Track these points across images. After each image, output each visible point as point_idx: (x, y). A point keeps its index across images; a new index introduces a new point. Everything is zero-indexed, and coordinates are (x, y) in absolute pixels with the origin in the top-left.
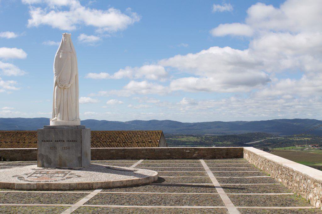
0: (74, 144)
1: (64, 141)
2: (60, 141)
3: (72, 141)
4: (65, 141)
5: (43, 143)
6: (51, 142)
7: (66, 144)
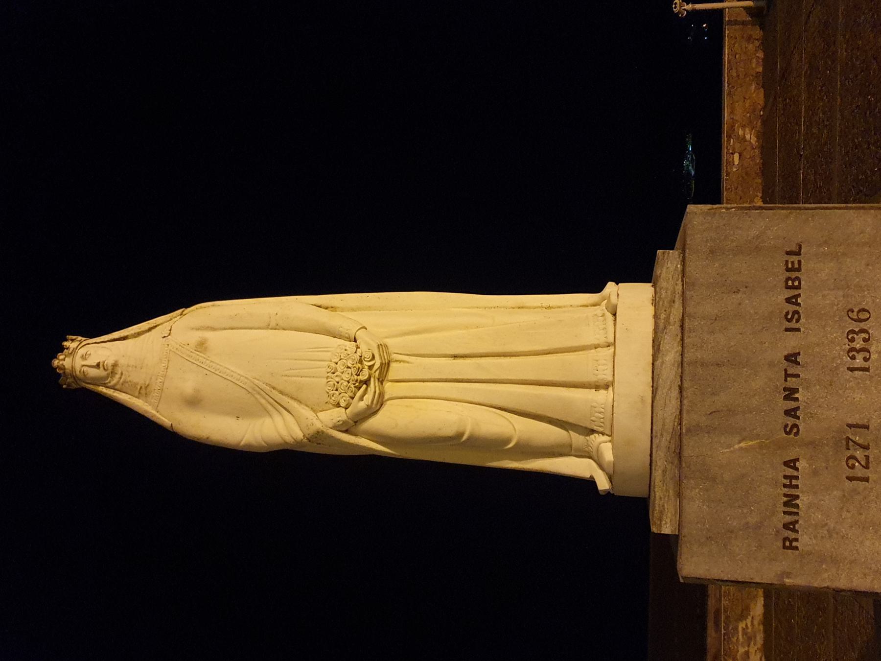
0: (816, 271)
1: (792, 358)
2: (790, 394)
3: (793, 284)
4: (791, 342)
5: (805, 540)
6: (801, 465)
7: (822, 339)
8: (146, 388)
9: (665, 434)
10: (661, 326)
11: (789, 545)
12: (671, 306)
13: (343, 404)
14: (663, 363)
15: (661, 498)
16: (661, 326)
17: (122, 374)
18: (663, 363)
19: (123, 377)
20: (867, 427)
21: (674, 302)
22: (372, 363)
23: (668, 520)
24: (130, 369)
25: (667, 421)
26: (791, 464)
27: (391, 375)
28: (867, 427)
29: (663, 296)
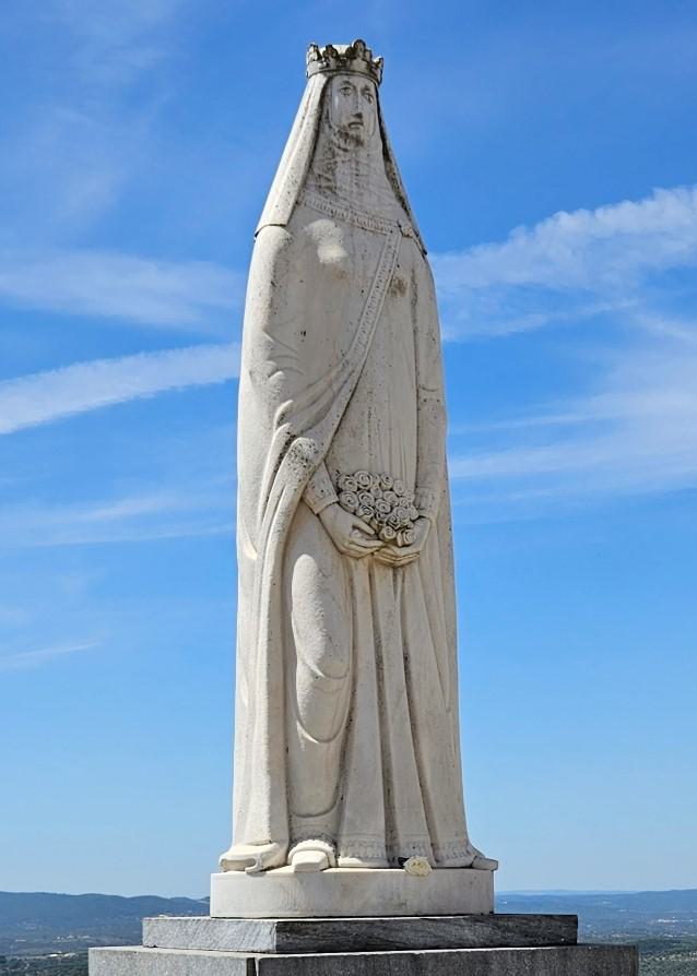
8: (329, 188)
9: (386, 932)
10: (501, 923)
12: (521, 932)
13: (344, 498)
14: (462, 926)
15: (315, 930)
16: (501, 923)
17: (345, 150)
18: (462, 926)
19: (341, 152)
20: (201, 907)
21: (526, 936)
22: (400, 543)
23: (291, 940)
24: (354, 166)
25: (401, 934)
27: (378, 572)
28: (201, 907)
29: (532, 924)
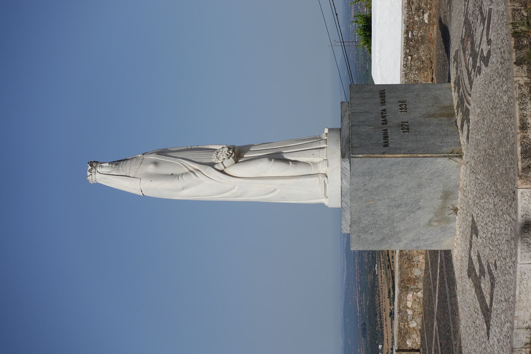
1: (384, 110)
4: (383, 107)
6: (388, 131)
11: (386, 145)
26: (386, 130)
